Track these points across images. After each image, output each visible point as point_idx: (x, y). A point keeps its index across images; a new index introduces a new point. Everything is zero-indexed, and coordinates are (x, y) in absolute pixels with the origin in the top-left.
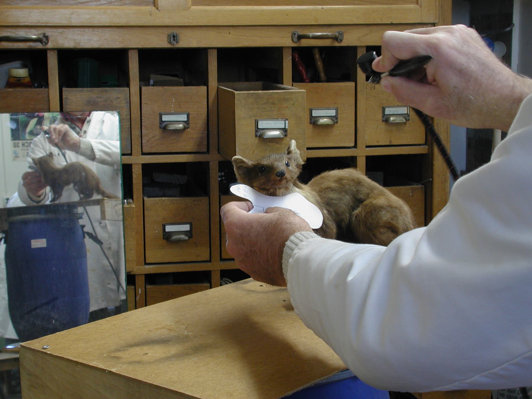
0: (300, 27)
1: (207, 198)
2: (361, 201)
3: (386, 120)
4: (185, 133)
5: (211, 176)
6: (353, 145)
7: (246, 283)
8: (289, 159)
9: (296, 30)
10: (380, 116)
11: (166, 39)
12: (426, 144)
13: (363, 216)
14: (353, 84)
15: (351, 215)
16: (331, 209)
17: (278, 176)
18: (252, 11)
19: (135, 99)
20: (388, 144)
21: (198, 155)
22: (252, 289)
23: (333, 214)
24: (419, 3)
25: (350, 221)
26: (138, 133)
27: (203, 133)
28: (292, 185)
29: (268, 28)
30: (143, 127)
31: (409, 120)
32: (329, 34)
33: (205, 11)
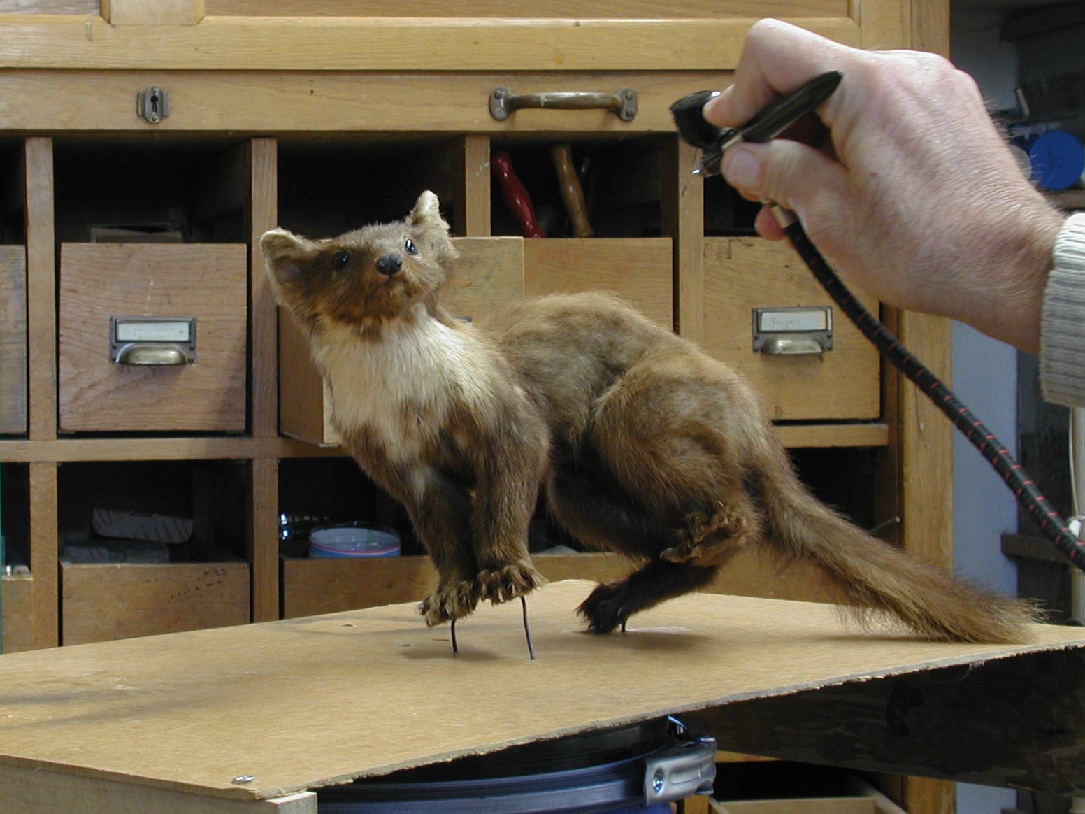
0: (512, 77)
1: (246, 565)
2: (619, 370)
3: (766, 350)
4: (182, 376)
5: (255, 500)
7: (308, 621)
8: (418, 237)
9: (502, 86)
10: (746, 336)
11: (129, 104)
13: (624, 403)
16: (538, 390)
17: (381, 269)
18: (377, 30)
19: (42, 277)
21: (218, 441)
23: (543, 404)
24: (855, 13)
26: (50, 374)
27: (234, 378)
29: (422, 77)
30: (62, 358)
31: (830, 349)
32: (596, 95)
33: (244, 28)
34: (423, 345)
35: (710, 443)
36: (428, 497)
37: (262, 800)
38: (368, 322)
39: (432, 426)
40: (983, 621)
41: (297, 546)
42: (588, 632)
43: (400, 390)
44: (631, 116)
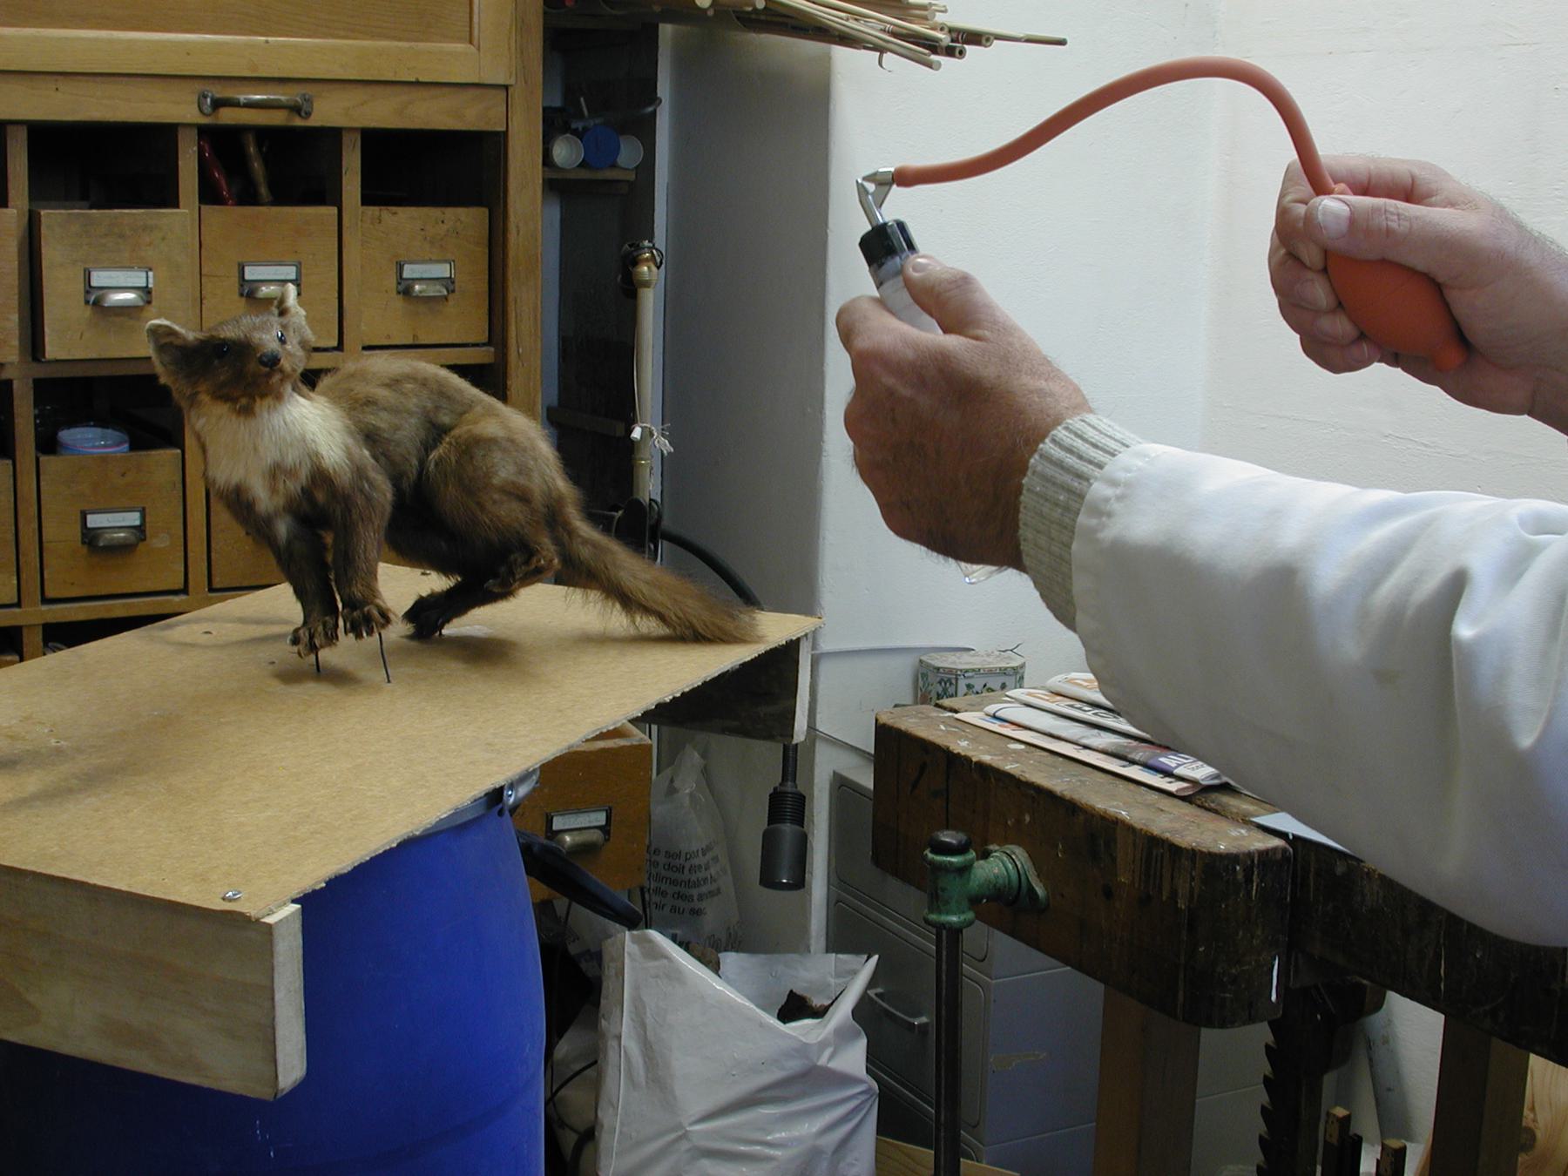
3: (406, 291)
6: (335, 343)
7: (170, 627)
8: (284, 327)
10: (392, 282)
12: (489, 343)
14: (335, 210)
15: (422, 463)
17: (265, 364)
18: (110, 41)
20: (410, 342)
22: (188, 640)
25: (420, 473)
28: (289, 388)
32: (283, 98)
34: (288, 418)
35: (523, 497)
36: (289, 542)
37: (257, 920)
38: (244, 401)
39: (294, 487)
40: (729, 626)
41: (48, 445)
42: (411, 637)
43: (269, 455)
44: (308, 114)
